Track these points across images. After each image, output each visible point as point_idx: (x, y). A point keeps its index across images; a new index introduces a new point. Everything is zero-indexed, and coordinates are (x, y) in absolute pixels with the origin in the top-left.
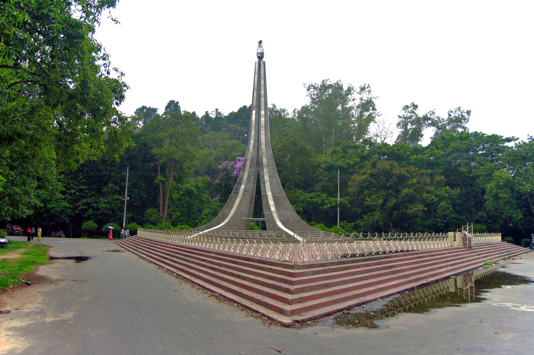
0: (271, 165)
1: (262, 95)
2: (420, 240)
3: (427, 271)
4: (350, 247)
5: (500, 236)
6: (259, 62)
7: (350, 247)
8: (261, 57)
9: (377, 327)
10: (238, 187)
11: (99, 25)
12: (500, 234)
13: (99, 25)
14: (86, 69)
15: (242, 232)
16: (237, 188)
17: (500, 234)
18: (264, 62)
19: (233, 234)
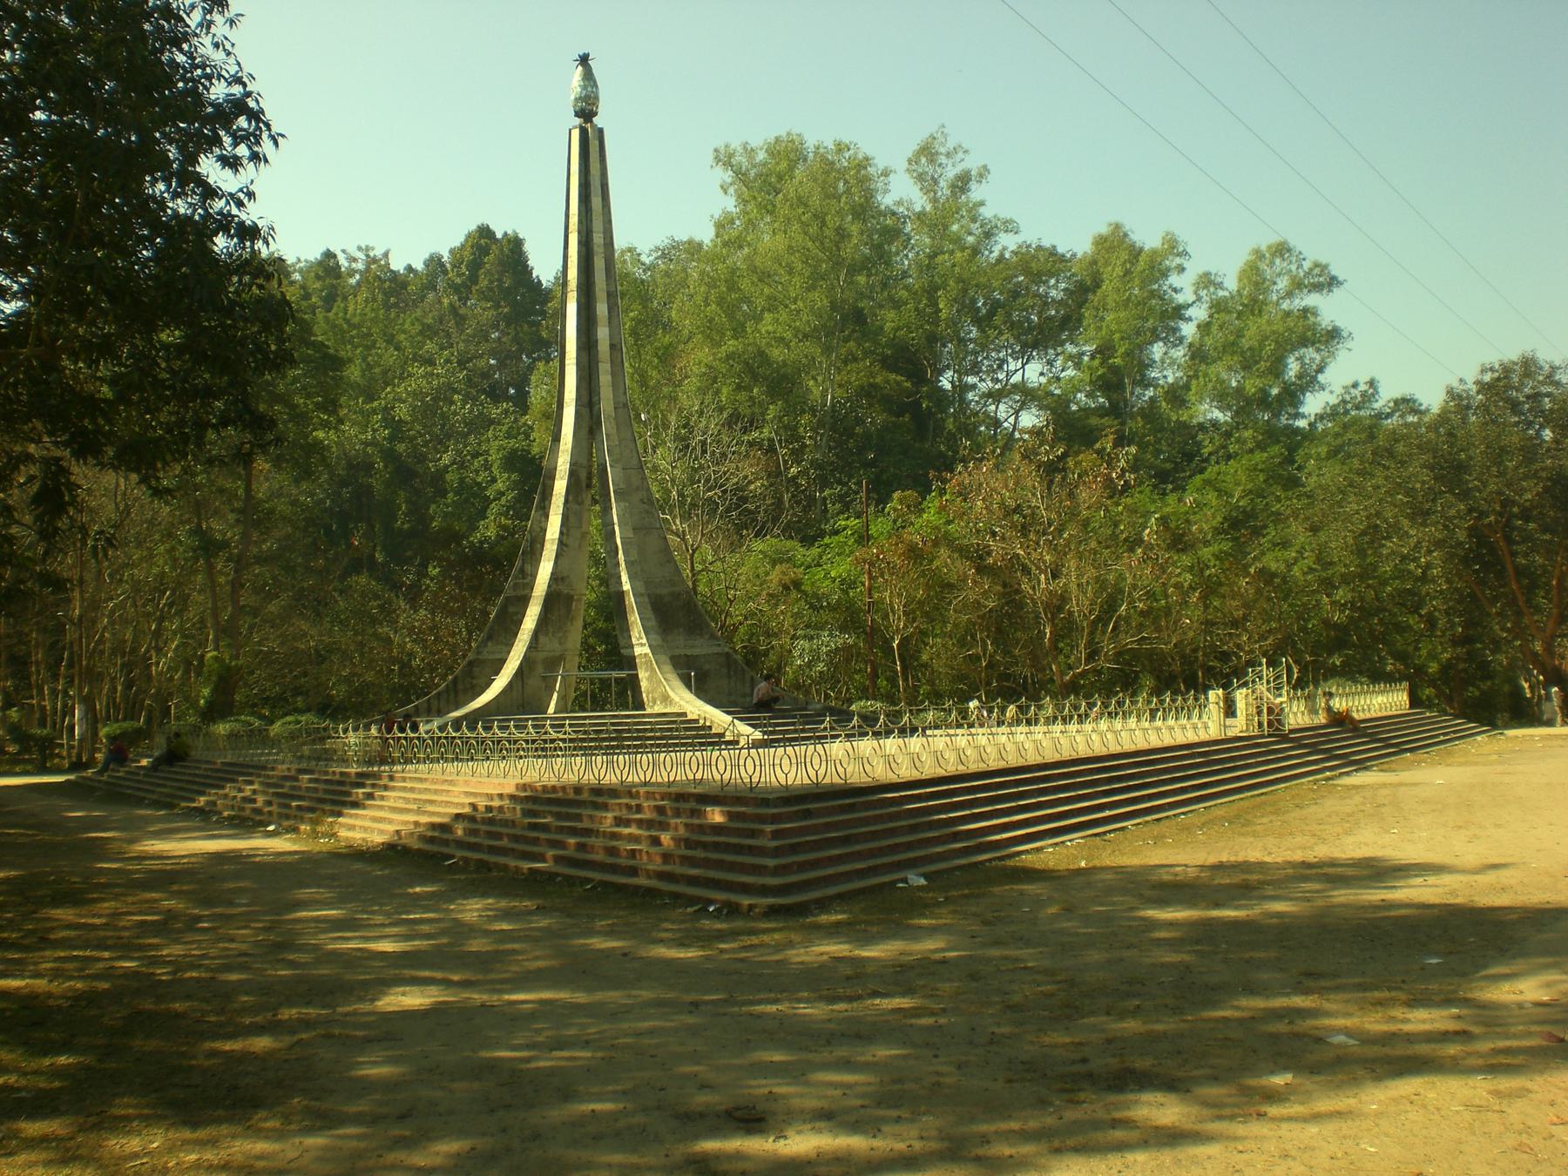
0: (638, 489)
1: (596, 248)
2: (1153, 717)
3: (832, 861)
4: (851, 752)
5: (1403, 690)
6: (584, 133)
7: (851, 752)
8: (586, 112)
9: (760, 1120)
10: (528, 568)
11: (283, 136)
12: (1405, 684)
13: (283, 136)
14: (923, 510)
15: (527, 720)
16: (522, 571)
17: (1405, 684)
18: (601, 131)
19: (534, 726)
